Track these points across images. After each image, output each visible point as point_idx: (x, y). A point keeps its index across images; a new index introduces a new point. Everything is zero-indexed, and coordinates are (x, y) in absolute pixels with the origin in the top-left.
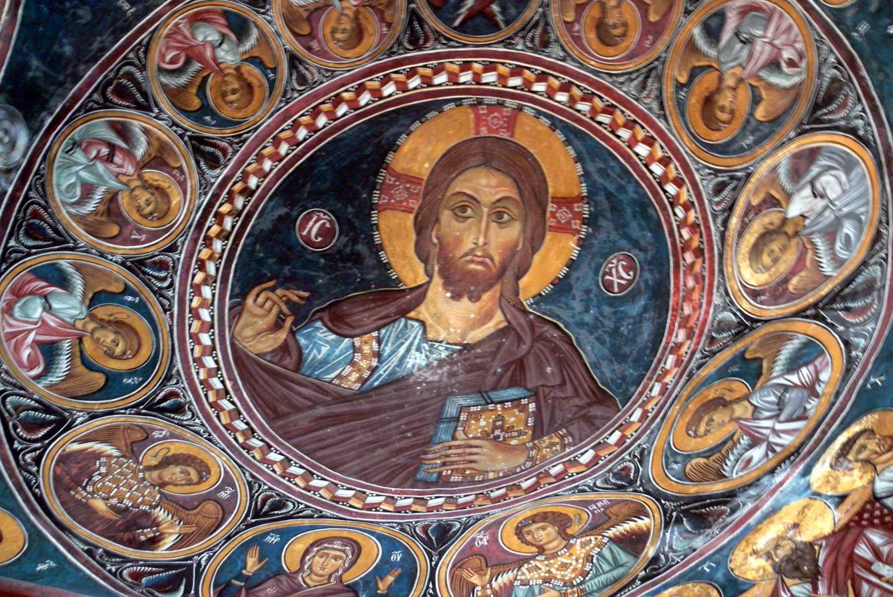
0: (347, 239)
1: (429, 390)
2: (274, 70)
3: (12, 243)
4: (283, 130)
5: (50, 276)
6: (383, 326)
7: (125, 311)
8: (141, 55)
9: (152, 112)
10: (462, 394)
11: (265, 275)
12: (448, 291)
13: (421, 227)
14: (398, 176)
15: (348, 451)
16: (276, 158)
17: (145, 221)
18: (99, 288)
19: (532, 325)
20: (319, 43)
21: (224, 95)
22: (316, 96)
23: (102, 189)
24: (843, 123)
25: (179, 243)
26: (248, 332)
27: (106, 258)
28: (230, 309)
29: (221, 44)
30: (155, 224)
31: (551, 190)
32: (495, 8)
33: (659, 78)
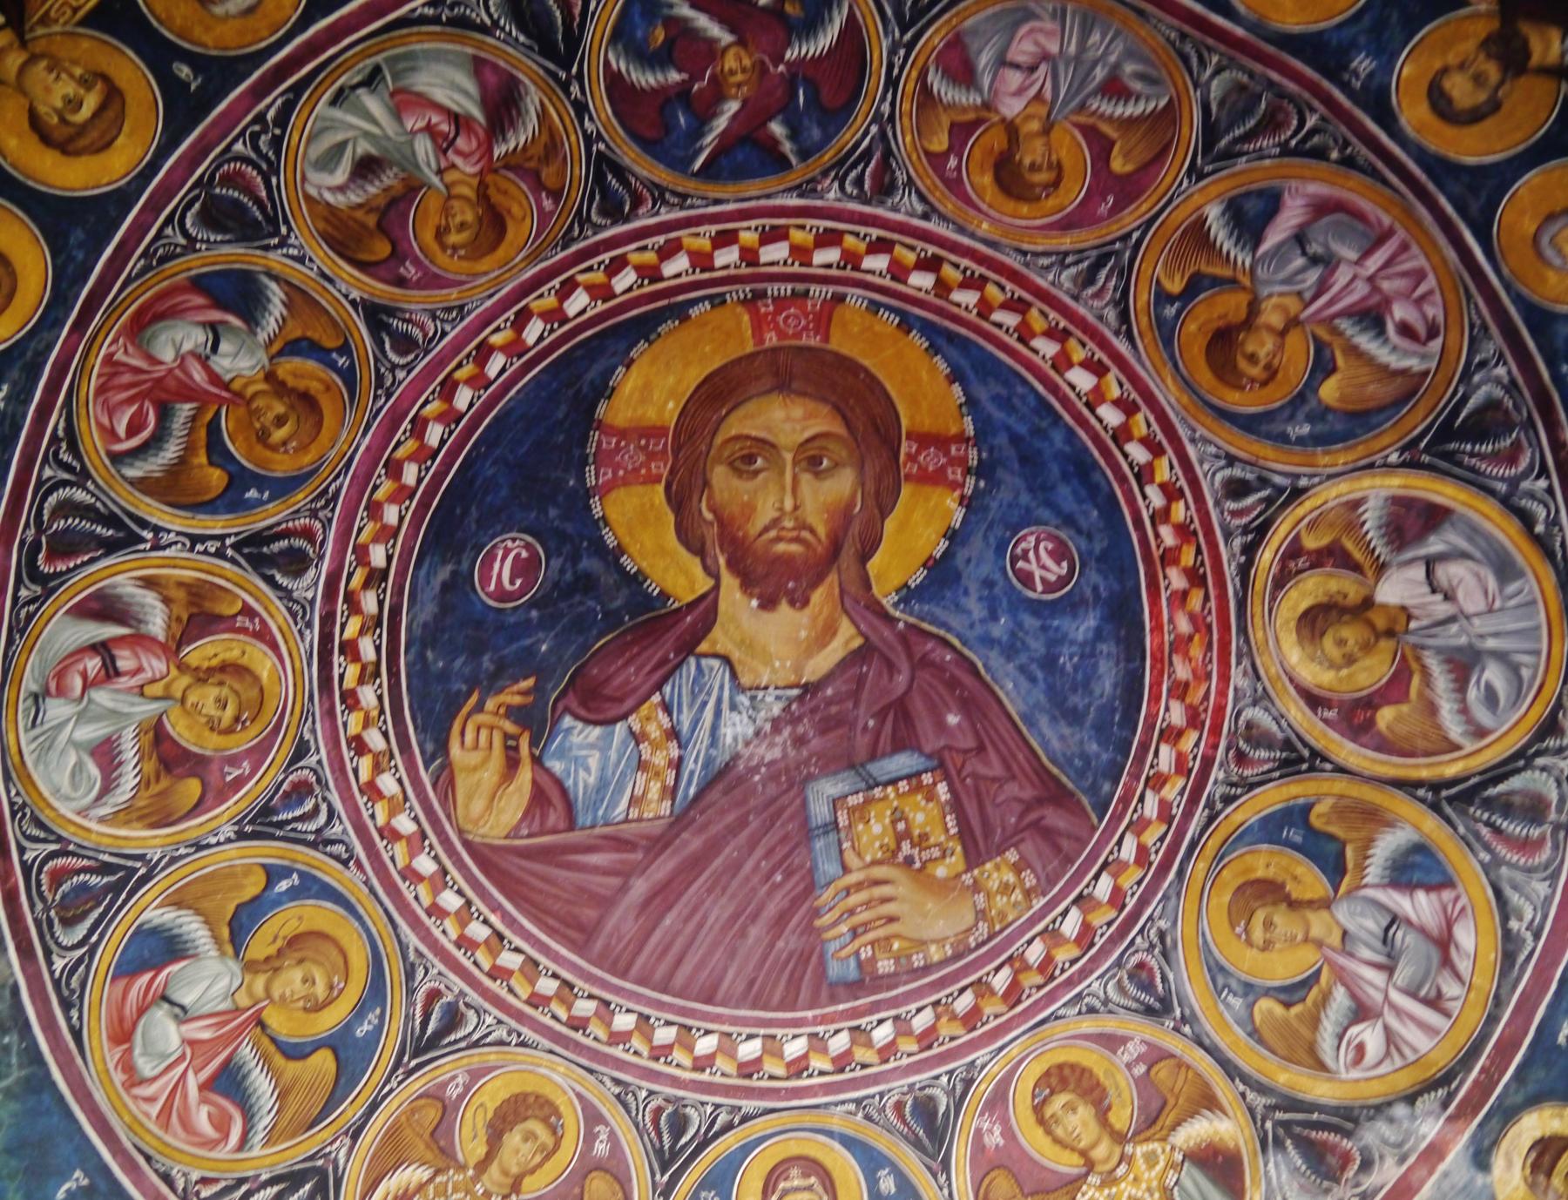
0: (561, 560)
1: (773, 777)
2: (345, 349)
3: (59, 964)
4: (399, 444)
5: (146, 953)
6: (665, 680)
7: (289, 914)
8: (66, 457)
9: (143, 540)
10: (827, 775)
11: (459, 691)
12: (751, 596)
13: (679, 501)
14: (623, 434)
15: (709, 953)
16: (402, 494)
17: (233, 738)
18: (231, 908)
19: (903, 638)
20: (417, 262)
21: (263, 437)
22: (441, 362)
23: (129, 734)
24: (1502, 487)
25: (307, 736)
26: (478, 806)
27: (208, 846)
28: (434, 786)
29: (215, 348)
30: (253, 731)
31: (905, 423)
32: (777, 128)
33: (1124, 273)
